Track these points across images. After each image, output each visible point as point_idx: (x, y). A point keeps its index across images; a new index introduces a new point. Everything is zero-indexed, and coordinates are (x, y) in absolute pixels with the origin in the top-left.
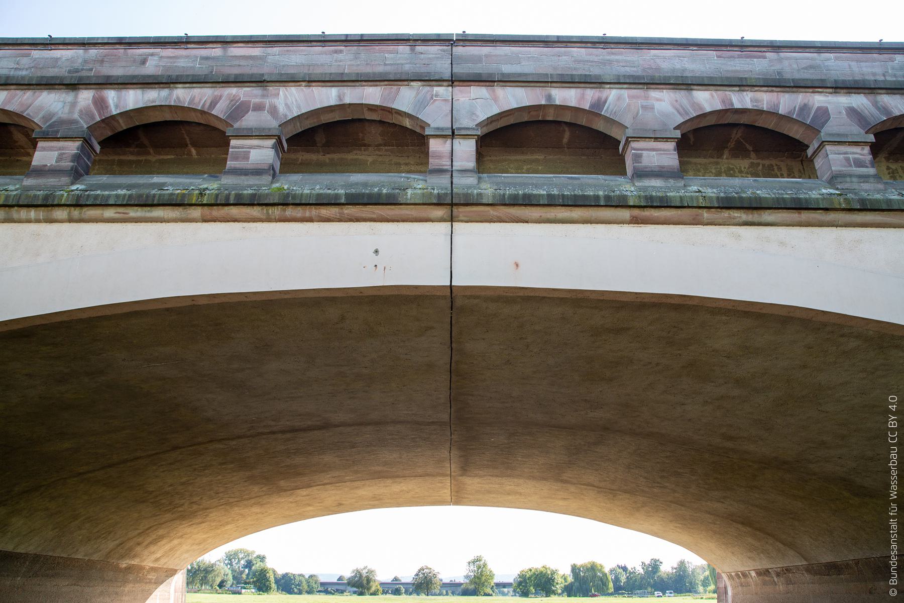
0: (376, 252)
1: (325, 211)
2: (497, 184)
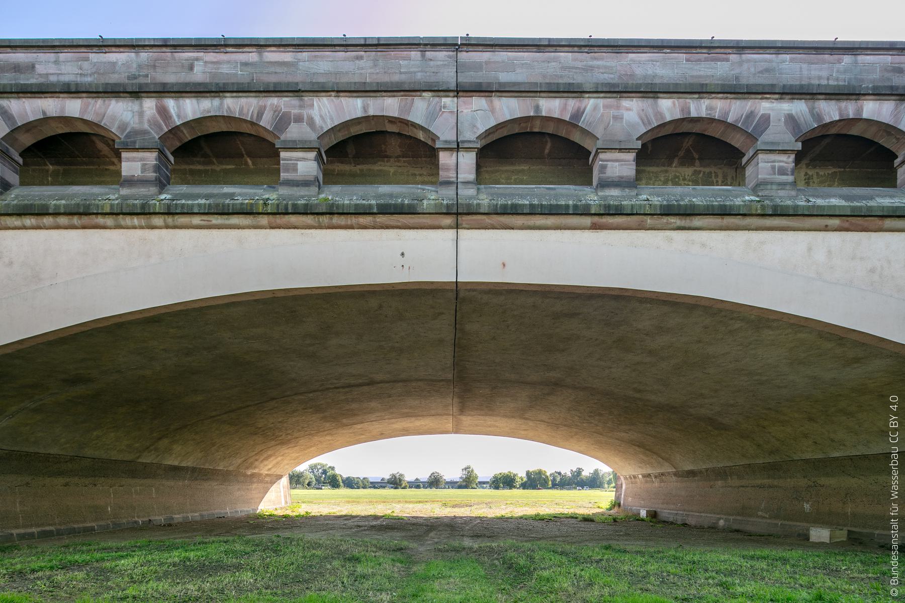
0: (403, 254)
1: (363, 220)
2: (492, 195)
